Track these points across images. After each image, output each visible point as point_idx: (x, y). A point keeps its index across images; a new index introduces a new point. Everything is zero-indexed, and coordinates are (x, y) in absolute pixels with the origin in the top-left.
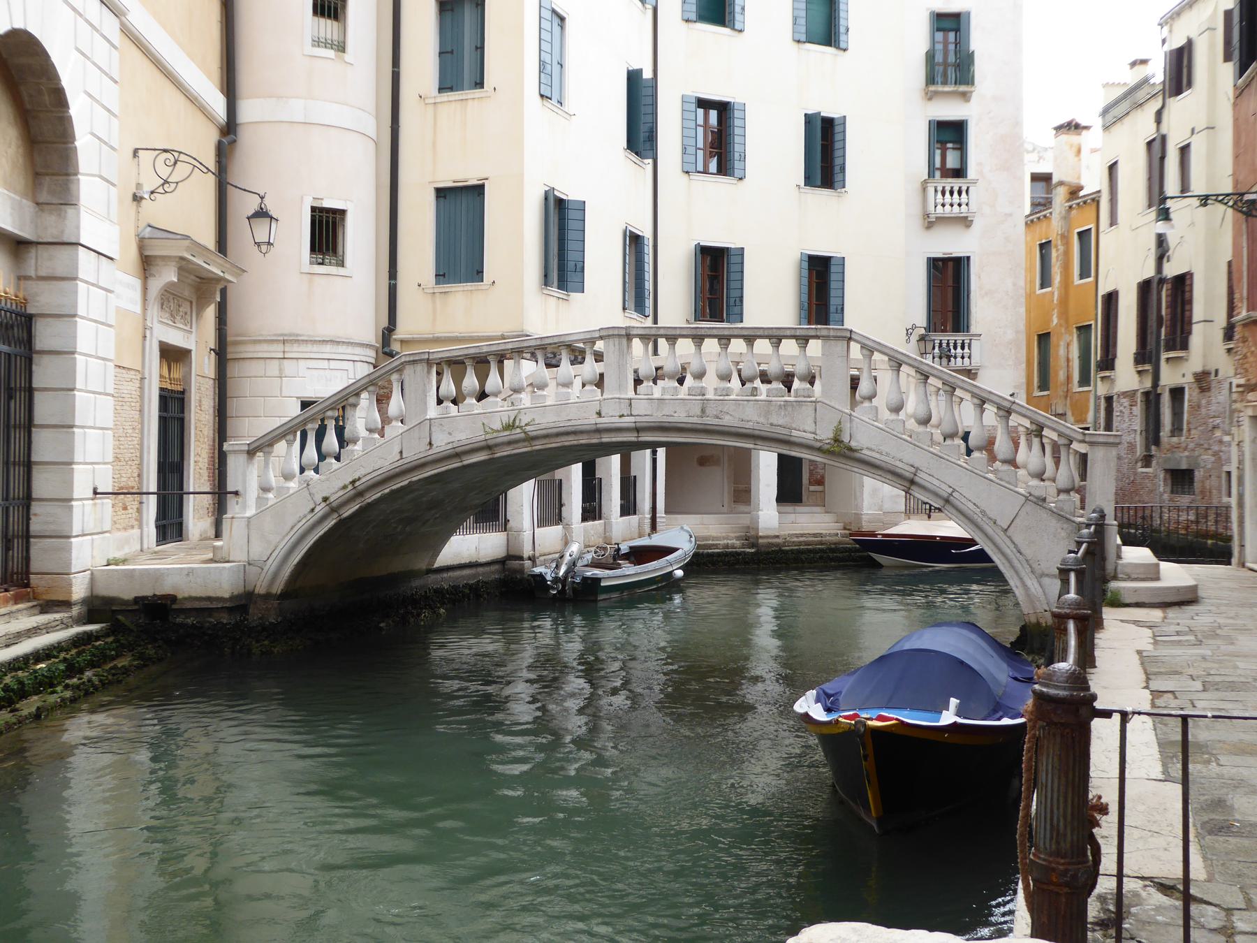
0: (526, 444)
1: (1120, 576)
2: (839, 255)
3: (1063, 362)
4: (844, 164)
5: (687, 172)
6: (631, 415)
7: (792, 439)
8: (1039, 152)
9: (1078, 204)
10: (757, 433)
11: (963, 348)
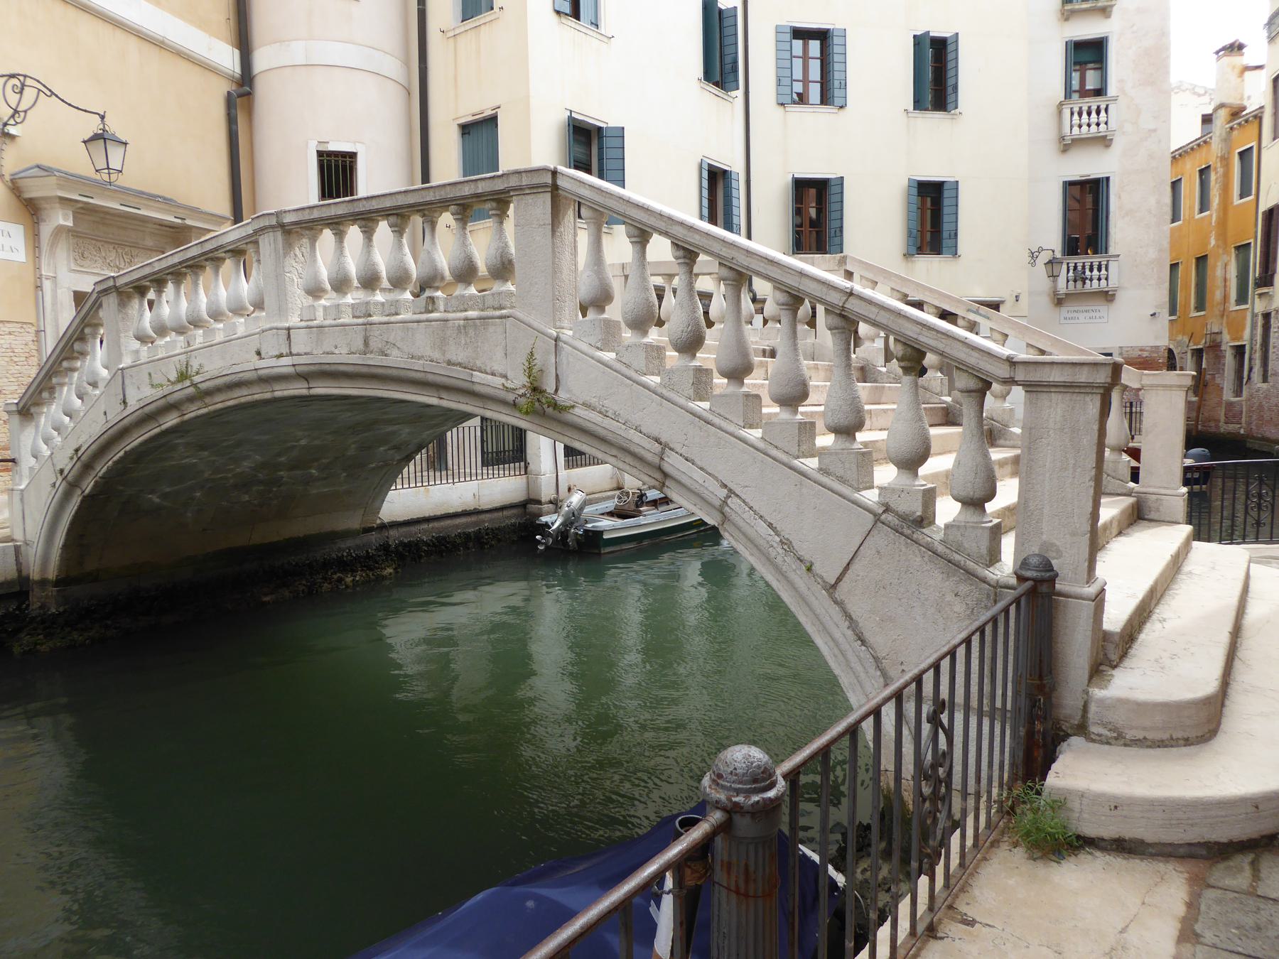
0: (198, 404)
1: (1094, 729)
2: (952, 180)
3: (1220, 283)
4: (957, 83)
5: (782, 104)
6: (291, 354)
7: (477, 388)
8: (1210, 94)
9: (1239, 124)
10: (430, 378)
11: (1099, 270)
